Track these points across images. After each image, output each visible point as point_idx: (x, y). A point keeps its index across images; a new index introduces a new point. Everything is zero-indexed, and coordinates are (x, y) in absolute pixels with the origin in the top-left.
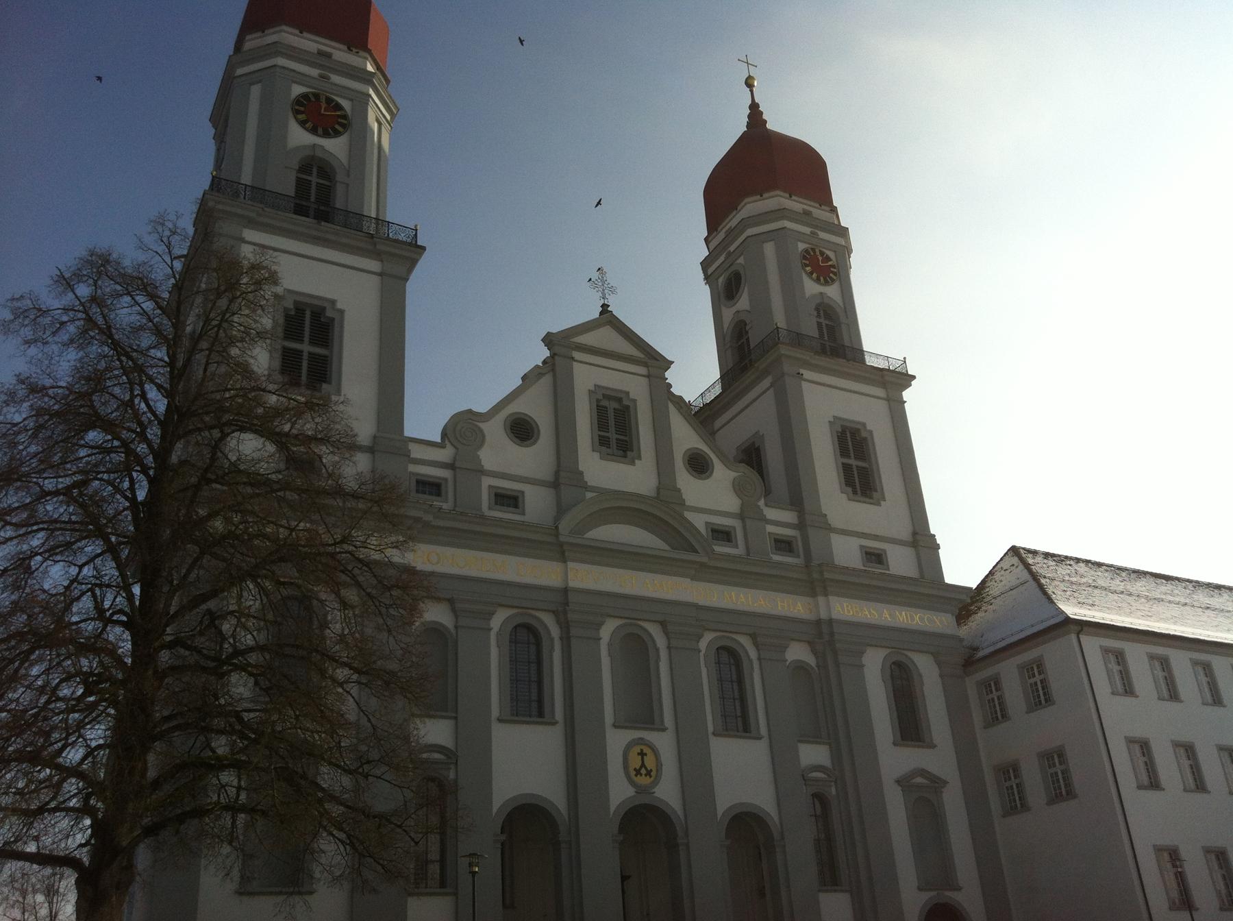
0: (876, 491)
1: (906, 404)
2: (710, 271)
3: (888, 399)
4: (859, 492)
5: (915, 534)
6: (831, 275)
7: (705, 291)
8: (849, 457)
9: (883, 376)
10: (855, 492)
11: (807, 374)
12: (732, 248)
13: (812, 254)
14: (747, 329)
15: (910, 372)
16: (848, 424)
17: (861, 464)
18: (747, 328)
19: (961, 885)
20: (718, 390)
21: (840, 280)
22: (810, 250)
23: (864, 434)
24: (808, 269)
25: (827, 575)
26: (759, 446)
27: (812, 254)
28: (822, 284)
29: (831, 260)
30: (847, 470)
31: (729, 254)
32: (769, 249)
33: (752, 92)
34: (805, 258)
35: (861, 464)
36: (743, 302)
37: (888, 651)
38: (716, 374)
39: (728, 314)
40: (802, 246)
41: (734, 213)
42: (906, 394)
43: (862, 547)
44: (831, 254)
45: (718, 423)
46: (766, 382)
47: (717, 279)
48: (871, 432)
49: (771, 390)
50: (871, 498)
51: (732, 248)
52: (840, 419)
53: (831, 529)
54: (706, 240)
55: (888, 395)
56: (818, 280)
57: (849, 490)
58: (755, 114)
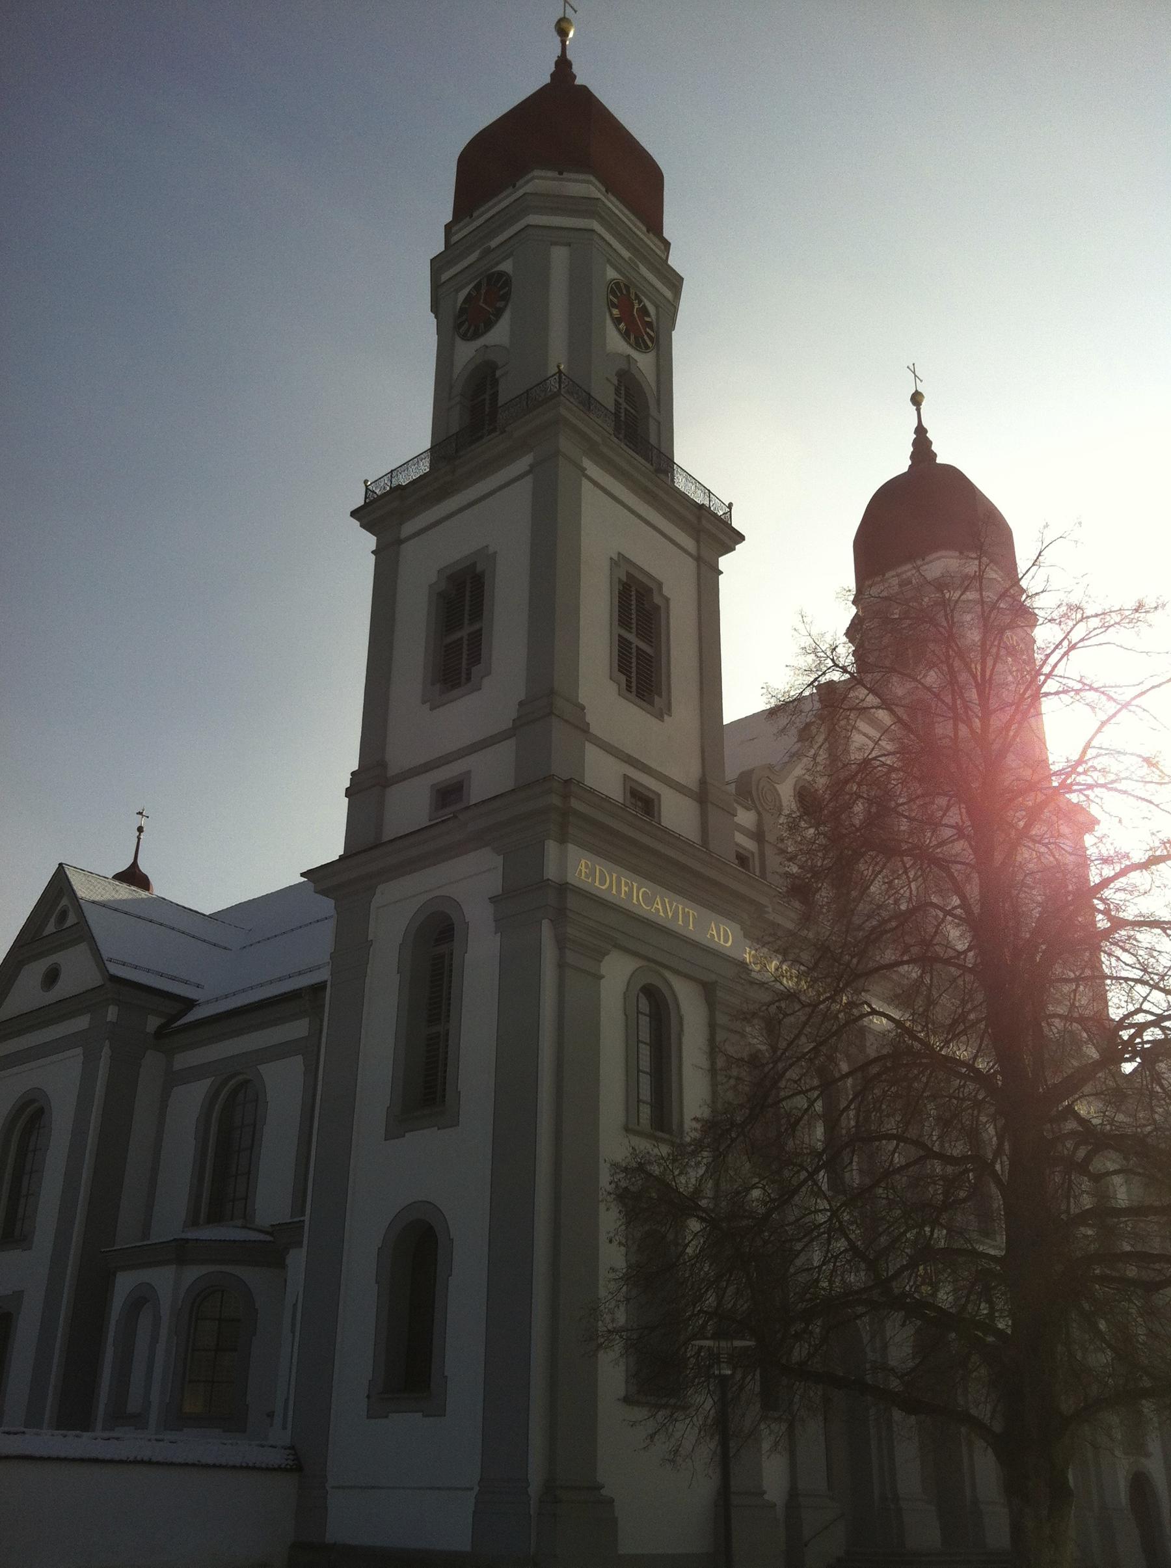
0: (660, 695)
1: (721, 577)
2: (445, 277)
3: (698, 559)
4: (634, 689)
5: (703, 782)
6: (473, 328)
7: (429, 323)
8: (629, 630)
9: (699, 518)
10: (629, 688)
11: (593, 470)
12: (493, 244)
13: (625, 292)
14: (497, 376)
15: (736, 524)
16: (640, 577)
17: (643, 646)
18: (498, 373)
19: (288, 1261)
20: (424, 467)
21: (658, 350)
22: (622, 285)
23: (657, 600)
24: (615, 312)
25: (575, 804)
26: (496, 553)
27: (625, 292)
28: (629, 343)
29: (649, 316)
30: (623, 650)
31: (488, 251)
32: (559, 256)
33: (918, 410)
34: (613, 292)
35: (643, 646)
36: (499, 334)
37: (641, 963)
38: (424, 442)
39: (466, 352)
40: (611, 274)
41: (403, 480)
42: (724, 562)
43: (626, 777)
44: (651, 309)
45: (408, 528)
46: (523, 463)
47: (457, 291)
48: (667, 600)
49: (529, 478)
50: (651, 703)
51: (493, 244)
52: (628, 561)
53: (584, 729)
54: (448, 227)
55: (699, 554)
56: (626, 335)
57: (623, 678)
58: (563, 66)
